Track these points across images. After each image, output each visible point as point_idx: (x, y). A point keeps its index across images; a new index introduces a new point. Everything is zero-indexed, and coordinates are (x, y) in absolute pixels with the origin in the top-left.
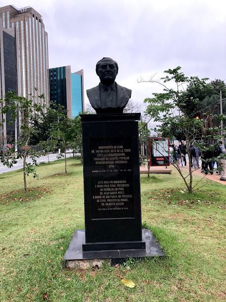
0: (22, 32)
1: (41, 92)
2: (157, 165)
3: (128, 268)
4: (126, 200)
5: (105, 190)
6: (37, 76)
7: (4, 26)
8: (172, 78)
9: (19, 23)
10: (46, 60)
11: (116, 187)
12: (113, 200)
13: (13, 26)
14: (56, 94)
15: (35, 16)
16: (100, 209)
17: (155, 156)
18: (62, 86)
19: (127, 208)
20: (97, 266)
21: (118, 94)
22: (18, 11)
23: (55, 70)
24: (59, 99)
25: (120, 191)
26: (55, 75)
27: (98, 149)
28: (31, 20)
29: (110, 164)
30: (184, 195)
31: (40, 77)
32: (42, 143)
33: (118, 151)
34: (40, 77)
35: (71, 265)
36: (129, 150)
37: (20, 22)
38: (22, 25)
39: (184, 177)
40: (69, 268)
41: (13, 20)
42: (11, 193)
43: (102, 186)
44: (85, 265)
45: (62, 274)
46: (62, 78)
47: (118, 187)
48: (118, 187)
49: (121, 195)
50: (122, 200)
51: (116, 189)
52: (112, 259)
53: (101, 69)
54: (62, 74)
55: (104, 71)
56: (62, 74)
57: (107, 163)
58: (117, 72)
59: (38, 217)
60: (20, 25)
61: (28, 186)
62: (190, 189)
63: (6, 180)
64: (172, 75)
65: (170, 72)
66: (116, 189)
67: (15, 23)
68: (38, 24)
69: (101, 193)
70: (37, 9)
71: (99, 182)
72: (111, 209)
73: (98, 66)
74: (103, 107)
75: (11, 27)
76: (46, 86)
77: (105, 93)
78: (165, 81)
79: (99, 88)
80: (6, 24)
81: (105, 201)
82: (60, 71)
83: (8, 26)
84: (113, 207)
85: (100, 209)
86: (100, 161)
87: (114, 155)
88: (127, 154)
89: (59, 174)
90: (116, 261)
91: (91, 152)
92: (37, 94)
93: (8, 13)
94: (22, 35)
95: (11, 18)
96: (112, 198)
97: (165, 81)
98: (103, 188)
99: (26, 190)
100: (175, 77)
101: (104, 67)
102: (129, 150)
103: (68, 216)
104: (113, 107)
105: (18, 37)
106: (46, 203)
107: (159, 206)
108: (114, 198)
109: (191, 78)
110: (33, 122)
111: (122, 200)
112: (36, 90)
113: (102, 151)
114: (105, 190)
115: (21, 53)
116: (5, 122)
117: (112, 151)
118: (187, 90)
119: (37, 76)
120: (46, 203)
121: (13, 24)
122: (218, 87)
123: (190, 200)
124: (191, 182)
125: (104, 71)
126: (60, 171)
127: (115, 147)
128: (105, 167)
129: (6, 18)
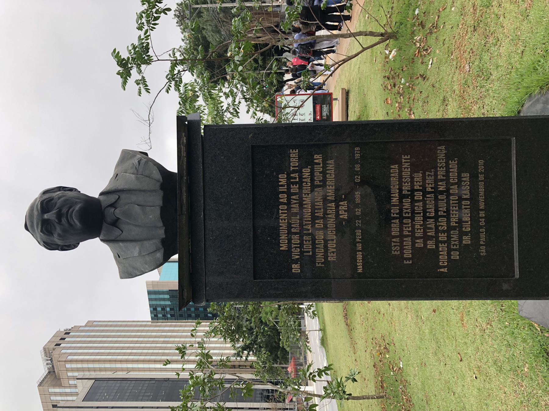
0: (85, 366)
1: (174, 355)
4: (454, 165)
6: (164, 342)
7: (74, 398)
8: (140, 72)
9: (69, 371)
10: (136, 326)
11: (412, 196)
15: (57, 341)
16: (483, 251)
19: (481, 162)
21: (127, 187)
22: (49, 372)
23: (154, 310)
26: (163, 309)
28: (66, 349)
29: (337, 215)
30: (400, 49)
31: (166, 337)
32: (284, 342)
34: (166, 337)
36: (294, 154)
37: (68, 370)
38: (74, 366)
39: (361, 49)
41: (64, 382)
43: (408, 242)
46: (167, 296)
48: (413, 191)
49: (436, 181)
50: (454, 176)
51: (418, 196)
53: (56, 235)
54: (161, 296)
55: (58, 230)
56: (161, 296)
58: (71, 190)
60: (72, 370)
62: (385, 37)
64: (134, 71)
65: (125, 75)
66: (418, 196)
67: (69, 378)
68: (73, 337)
69: (431, 245)
70: (46, 336)
71: (395, 252)
72: (482, 214)
73: (50, 246)
74: (161, 233)
75: (75, 386)
76: (181, 326)
77: (123, 227)
78: (147, 90)
79: (116, 245)
80: (71, 394)
81: (455, 235)
82: (156, 300)
83: (73, 390)
84: (474, 209)
85: (483, 251)
86: (326, 247)
88: (307, 161)
89: (346, 316)
91: (296, 276)
93: (52, 390)
94: (97, 366)
95: (60, 386)
96: (448, 211)
97: (147, 90)
98: (414, 238)
99: (382, 397)
100: (139, 66)
102: (294, 154)
104: (160, 202)
105: (93, 375)
107: (432, 101)
108: (448, 203)
109: (140, 28)
110: (246, 352)
111: (454, 176)
113: (296, 239)
115: (122, 370)
119: (164, 342)
121: (71, 382)
122: (187, 12)
123: (413, 33)
124: (372, 34)
125: (58, 230)
127: (283, 198)
129: (61, 394)
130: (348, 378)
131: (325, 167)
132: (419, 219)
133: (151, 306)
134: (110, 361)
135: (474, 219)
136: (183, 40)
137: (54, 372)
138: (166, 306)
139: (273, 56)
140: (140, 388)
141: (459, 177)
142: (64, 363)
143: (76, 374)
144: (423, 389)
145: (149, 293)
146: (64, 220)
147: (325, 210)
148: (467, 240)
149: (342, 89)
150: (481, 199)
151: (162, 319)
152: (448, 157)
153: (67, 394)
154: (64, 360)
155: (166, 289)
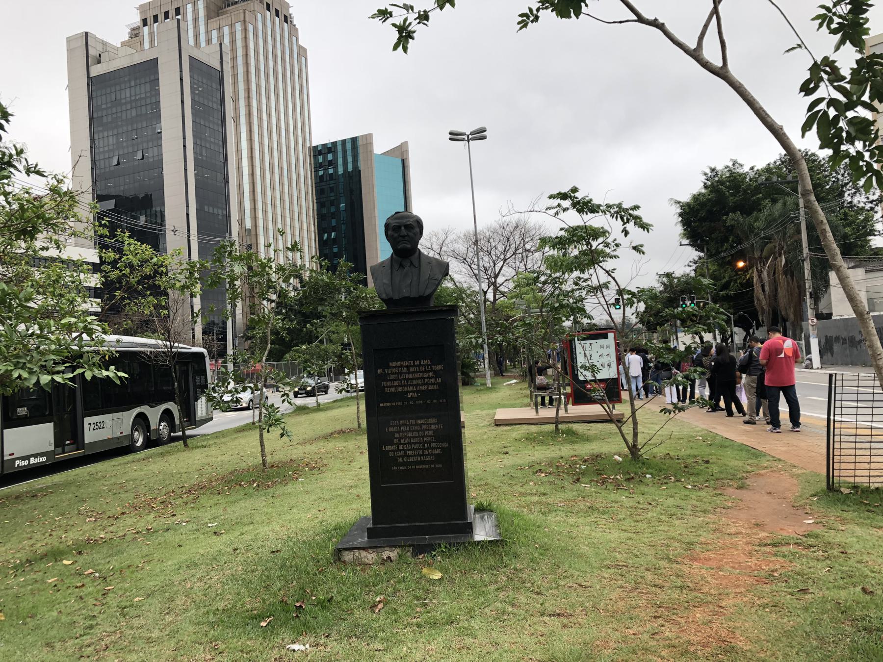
2: (591, 401)
3: (439, 558)
4: (439, 451)
5: (402, 435)
6: (281, 169)
7: (192, 41)
11: (421, 430)
12: (416, 453)
13: (215, 41)
14: (333, 216)
16: (395, 468)
17: (581, 378)
18: (352, 191)
20: (389, 558)
24: (344, 227)
25: (427, 436)
26: (330, 163)
27: (388, 367)
33: (422, 369)
35: (348, 556)
36: (440, 367)
37: (232, 26)
38: (239, 36)
40: (344, 562)
41: (214, 23)
42: (232, 473)
43: (397, 429)
44: (370, 557)
45: (332, 570)
46: (350, 167)
47: (424, 431)
48: (424, 431)
49: (430, 443)
50: (433, 451)
51: (421, 434)
52: (413, 546)
54: (350, 159)
55: (396, 235)
56: (350, 159)
57: (404, 389)
59: (294, 511)
60: (232, 34)
61: (268, 459)
62: (634, 449)
63: (213, 451)
66: (421, 434)
67: (220, 29)
68: (282, 29)
69: (396, 441)
72: (413, 467)
74: (396, 297)
76: (306, 193)
80: (197, 35)
82: (344, 151)
84: (416, 463)
85: (395, 468)
87: (416, 376)
89: (342, 432)
90: (419, 550)
92: (285, 242)
95: (208, 17)
96: (414, 449)
98: (399, 432)
101: (397, 228)
103: (353, 506)
105: (227, 68)
106: (308, 487)
111: (433, 451)
112: (282, 233)
113: (396, 370)
114: (402, 435)
115: (236, 109)
116: (198, 297)
117: (412, 369)
118: (706, 186)
120: (308, 487)
121: (214, 34)
124: (635, 435)
125: (396, 235)
126: (345, 426)
127: (417, 363)
128: (402, 396)
129: (196, 19)
130: (283, 429)
131: (435, 384)
132: (409, 434)
133: (334, 144)
134: (248, 90)
135: (411, 463)
136: (752, 168)
137: (228, 6)
138: (336, 168)
139: (734, 314)
140: (212, 140)
141: (432, 455)
142: (242, 19)
143: (227, 40)
144: (284, 494)
145: (354, 140)
146: (400, 239)
147: (412, 385)
148: (400, 459)
149: (623, 415)
150: (421, 467)
151: (315, 163)
152: (442, 449)
153: (196, 28)
154: (247, 19)
155: (362, 166)
